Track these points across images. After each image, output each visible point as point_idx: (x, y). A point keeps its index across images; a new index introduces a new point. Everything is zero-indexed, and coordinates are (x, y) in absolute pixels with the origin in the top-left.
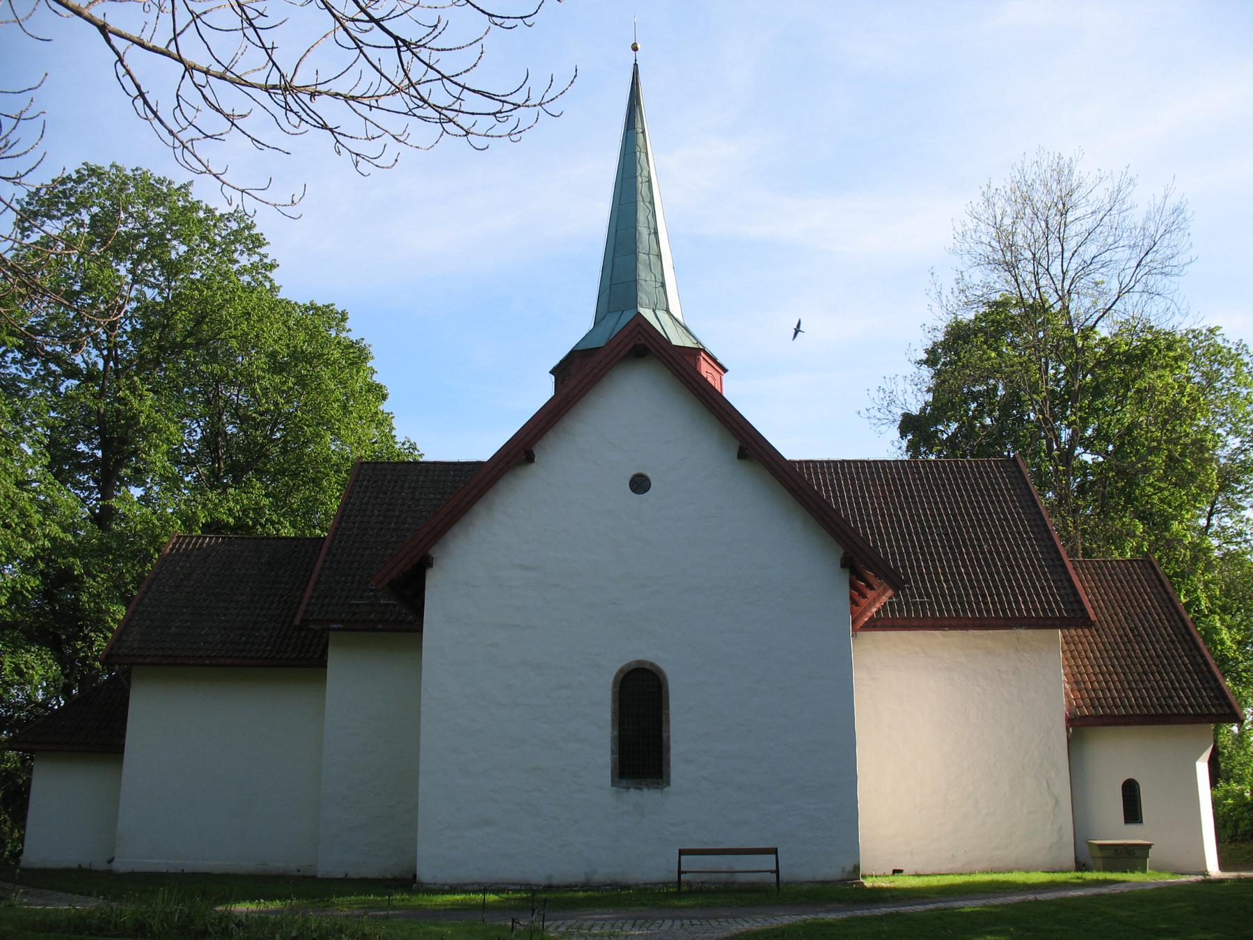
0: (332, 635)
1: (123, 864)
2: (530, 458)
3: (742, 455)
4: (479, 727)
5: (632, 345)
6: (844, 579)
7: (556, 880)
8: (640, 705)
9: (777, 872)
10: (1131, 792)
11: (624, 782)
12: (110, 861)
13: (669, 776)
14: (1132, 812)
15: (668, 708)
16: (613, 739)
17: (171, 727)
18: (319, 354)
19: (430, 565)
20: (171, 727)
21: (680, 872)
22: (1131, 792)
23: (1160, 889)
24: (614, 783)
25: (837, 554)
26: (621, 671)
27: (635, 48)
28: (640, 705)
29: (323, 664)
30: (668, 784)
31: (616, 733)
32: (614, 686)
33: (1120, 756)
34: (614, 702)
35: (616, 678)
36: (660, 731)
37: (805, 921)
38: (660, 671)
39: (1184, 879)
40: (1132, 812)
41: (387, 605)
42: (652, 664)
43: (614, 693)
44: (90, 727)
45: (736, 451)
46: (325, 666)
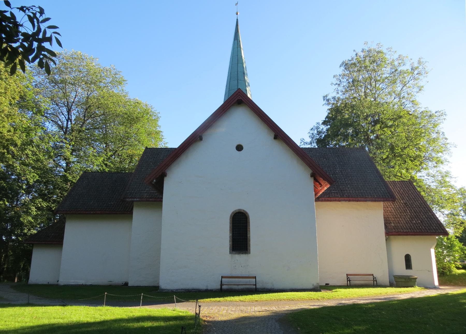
0: (135, 203)
1: (63, 281)
2: (201, 139)
3: (276, 138)
4: (183, 232)
5: (236, 100)
7: (209, 288)
8: (240, 225)
9: (256, 285)
10: (408, 259)
11: (234, 252)
12: (58, 281)
13: (250, 250)
14: (408, 264)
16: (230, 237)
17: (76, 233)
19: (166, 176)
21: (221, 285)
22: (408, 259)
24: (230, 253)
25: (310, 171)
26: (233, 213)
28: (240, 225)
29: (132, 213)
30: (250, 253)
31: (231, 235)
32: (230, 218)
33: (403, 246)
34: (230, 224)
36: (247, 234)
37: (360, 329)
40: (408, 264)
45: (273, 136)
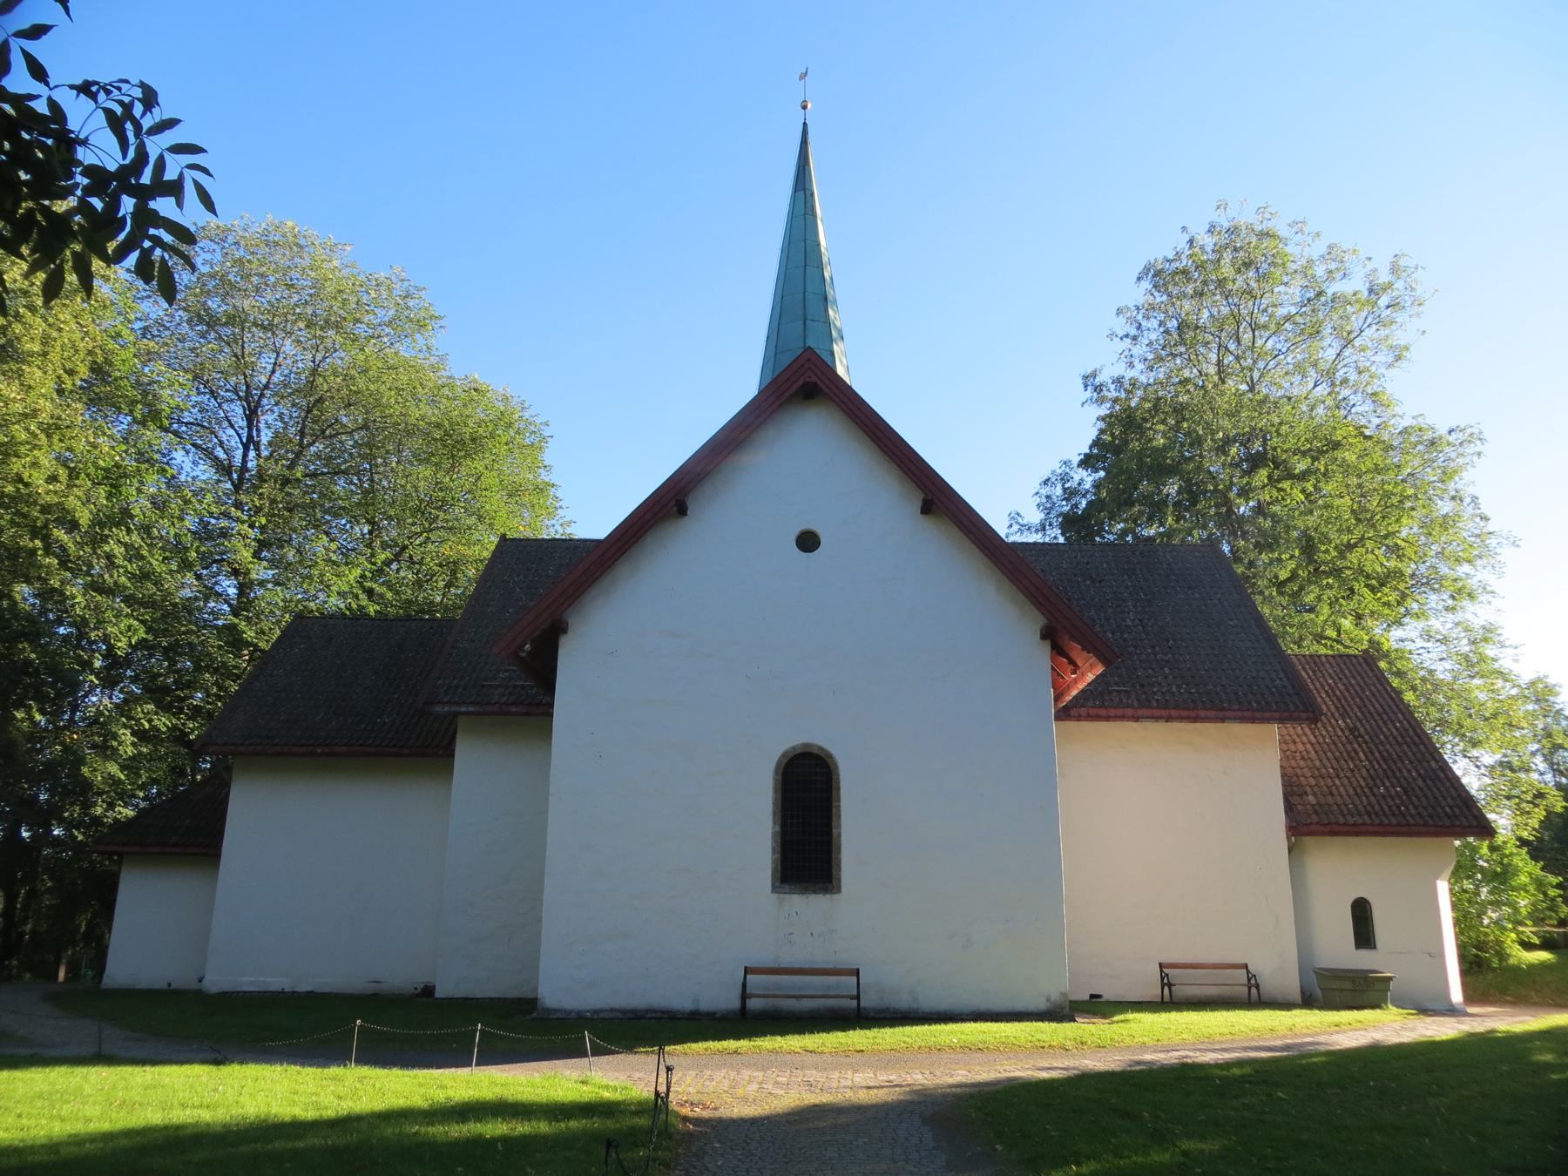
0: (461, 720)
1: (217, 980)
2: (682, 511)
3: (927, 509)
4: (620, 818)
5: (800, 383)
6: (1043, 653)
7: (705, 1006)
8: (807, 803)
10: (1362, 913)
11: (787, 887)
13: (839, 880)
14: (1364, 933)
15: (839, 800)
17: (270, 821)
18: (462, 439)
19: (565, 631)
20: (270, 821)
22: (1362, 913)
23: (1151, 1071)
24: (774, 889)
25: (1037, 621)
27: (805, 108)
29: (449, 753)
30: (839, 890)
31: (778, 828)
32: (776, 773)
33: (1347, 870)
34: (776, 792)
35: (779, 763)
38: (830, 756)
39: (1227, 1056)
40: (1364, 933)
41: (523, 687)
42: (820, 748)
43: (776, 781)
44: (186, 831)
46: (451, 755)
